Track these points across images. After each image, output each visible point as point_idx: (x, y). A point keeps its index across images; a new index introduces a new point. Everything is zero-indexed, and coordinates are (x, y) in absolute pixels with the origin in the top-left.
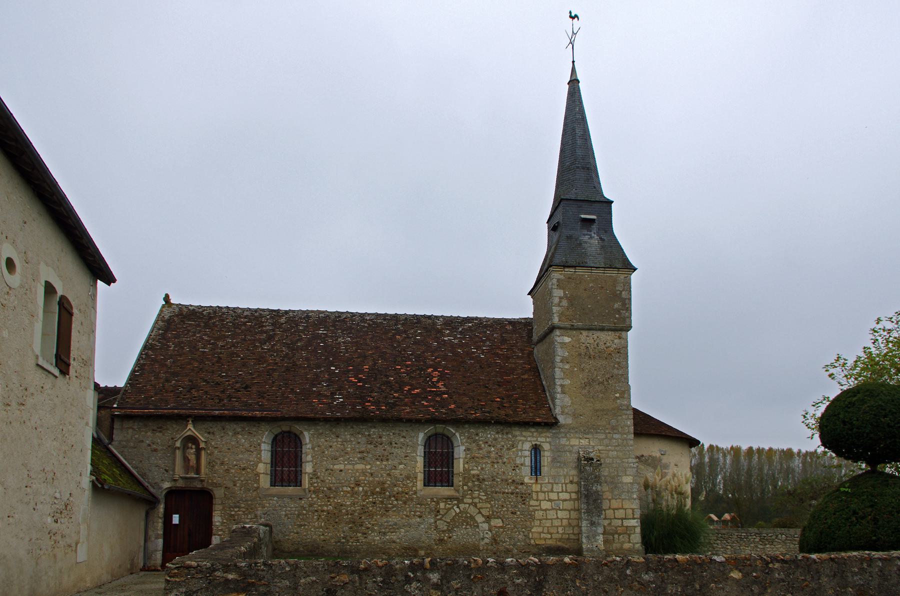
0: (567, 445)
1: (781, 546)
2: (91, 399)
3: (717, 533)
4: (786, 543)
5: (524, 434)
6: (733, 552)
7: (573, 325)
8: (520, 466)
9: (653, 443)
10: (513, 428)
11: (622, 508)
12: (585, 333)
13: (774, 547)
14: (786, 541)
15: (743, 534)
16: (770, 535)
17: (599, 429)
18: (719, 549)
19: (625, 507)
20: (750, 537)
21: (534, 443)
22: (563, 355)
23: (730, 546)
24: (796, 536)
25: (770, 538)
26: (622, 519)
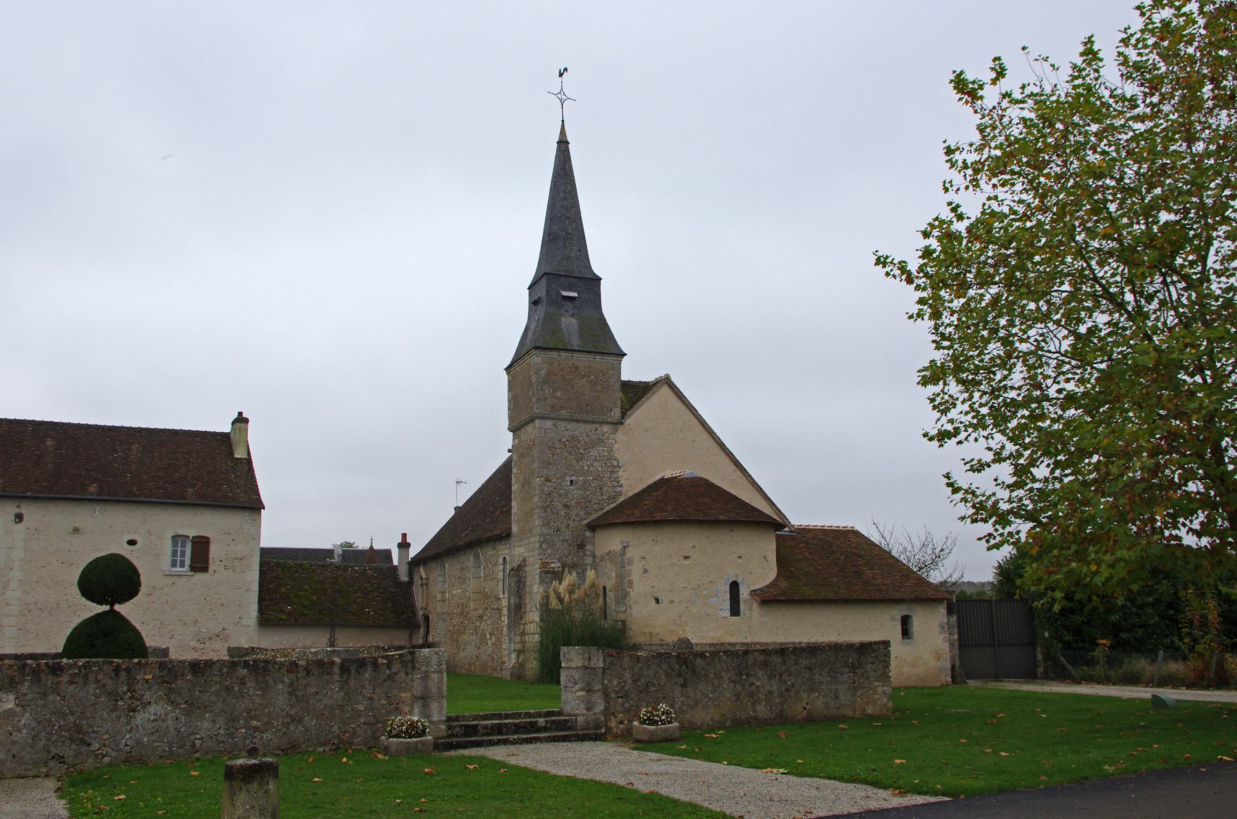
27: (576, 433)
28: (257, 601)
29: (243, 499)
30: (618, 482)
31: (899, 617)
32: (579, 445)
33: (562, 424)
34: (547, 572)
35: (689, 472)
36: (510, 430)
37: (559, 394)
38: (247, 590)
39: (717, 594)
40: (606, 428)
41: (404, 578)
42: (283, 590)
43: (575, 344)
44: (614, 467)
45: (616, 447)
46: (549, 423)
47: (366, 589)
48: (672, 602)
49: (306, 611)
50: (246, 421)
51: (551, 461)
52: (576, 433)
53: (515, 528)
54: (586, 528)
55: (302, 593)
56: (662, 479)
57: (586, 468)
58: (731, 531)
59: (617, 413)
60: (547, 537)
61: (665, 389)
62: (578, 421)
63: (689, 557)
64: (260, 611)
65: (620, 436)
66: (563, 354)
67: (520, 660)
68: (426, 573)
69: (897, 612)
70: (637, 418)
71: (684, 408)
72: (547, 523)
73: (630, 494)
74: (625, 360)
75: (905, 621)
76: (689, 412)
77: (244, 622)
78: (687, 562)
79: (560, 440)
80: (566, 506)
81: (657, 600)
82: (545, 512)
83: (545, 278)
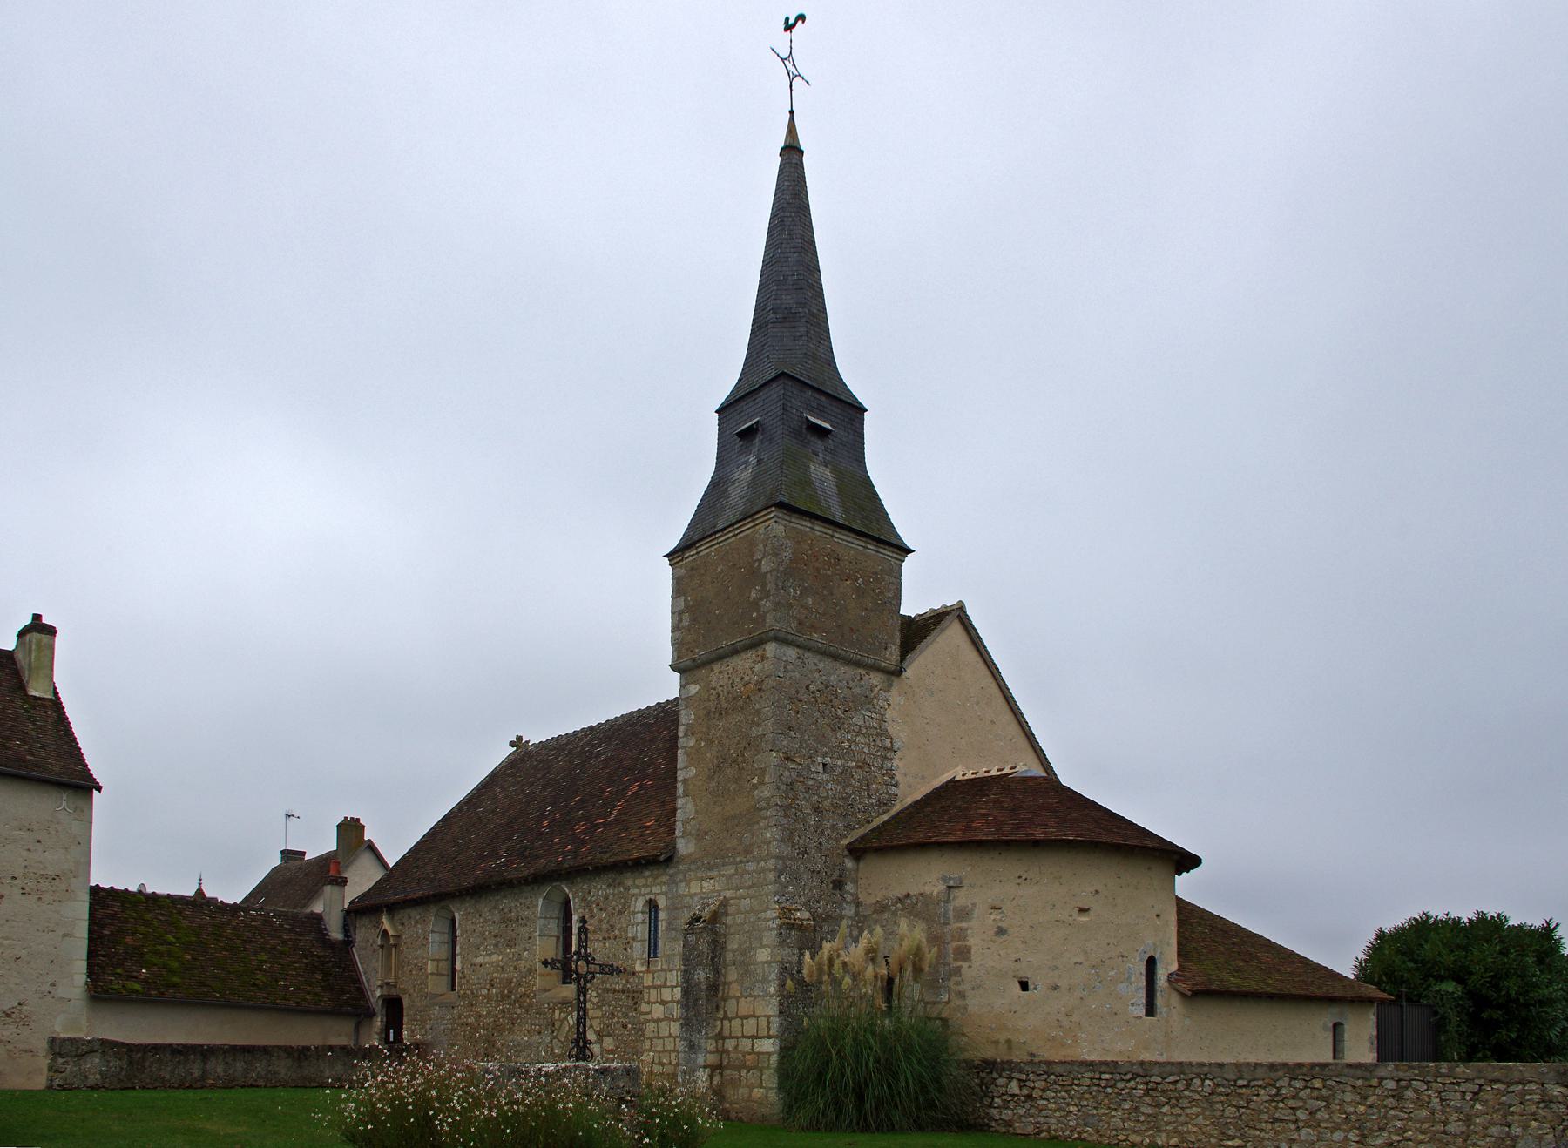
0: (686, 896)
1: (1199, 1110)
2: (80, 909)
3: (1045, 1073)
4: (1212, 1103)
5: (638, 882)
6: (1081, 1122)
7: (694, 660)
8: (631, 941)
9: (965, 860)
10: (625, 874)
11: (754, 1016)
12: (717, 667)
13: (1180, 1112)
14: (1215, 1098)
15: (1103, 1076)
16: (1171, 1079)
17: (728, 857)
18: (1050, 1112)
19: (757, 1013)
20: (1120, 1085)
21: (648, 897)
22: (687, 722)
23: (1075, 1105)
24: (1240, 1082)
25: (1171, 1087)
26: (753, 1038)
27: (832, 678)
28: (85, 957)
29: (57, 769)
30: (892, 778)
31: (1331, 1025)
32: (836, 702)
33: (811, 659)
34: (791, 927)
35: (1025, 768)
36: (674, 667)
37: (810, 601)
38: (65, 935)
39: (1129, 977)
40: (876, 679)
41: (336, 934)
42: (128, 939)
43: (837, 514)
44: (886, 748)
45: (889, 714)
46: (791, 653)
47: (274, 948)
48: (1055, 988)
49: (176, 979)
50: (51, 631)
51: (793, 724)
52: (832, 678)
53: (684, 847)
54: (846, 853)
55: (163, 948)
56: (951, 781)
57: (846, 745)
58: (1149, 869)
59: (894, 653)
60: (789, 863)
61: (954, 630)
62: (835, 657)
63: (1088, 910)
64: (91, 973)
65: (894, 696)
66: (820, 528)
67: (715, 1082)
68: (394, 927)
69: (1328, 1017)
70: (918, 666)
71: (981, 665)
72: (788, 839)
73: (909, 801)
74: (909, 564)
75: (1337, 1027)
76: (988, 673)
77: (61, 992)
78: (1084, 919)
79: (807, 688)
80: (817, 810)
81: (1024, 986)
82: (786, 816)
83: (776, 390)
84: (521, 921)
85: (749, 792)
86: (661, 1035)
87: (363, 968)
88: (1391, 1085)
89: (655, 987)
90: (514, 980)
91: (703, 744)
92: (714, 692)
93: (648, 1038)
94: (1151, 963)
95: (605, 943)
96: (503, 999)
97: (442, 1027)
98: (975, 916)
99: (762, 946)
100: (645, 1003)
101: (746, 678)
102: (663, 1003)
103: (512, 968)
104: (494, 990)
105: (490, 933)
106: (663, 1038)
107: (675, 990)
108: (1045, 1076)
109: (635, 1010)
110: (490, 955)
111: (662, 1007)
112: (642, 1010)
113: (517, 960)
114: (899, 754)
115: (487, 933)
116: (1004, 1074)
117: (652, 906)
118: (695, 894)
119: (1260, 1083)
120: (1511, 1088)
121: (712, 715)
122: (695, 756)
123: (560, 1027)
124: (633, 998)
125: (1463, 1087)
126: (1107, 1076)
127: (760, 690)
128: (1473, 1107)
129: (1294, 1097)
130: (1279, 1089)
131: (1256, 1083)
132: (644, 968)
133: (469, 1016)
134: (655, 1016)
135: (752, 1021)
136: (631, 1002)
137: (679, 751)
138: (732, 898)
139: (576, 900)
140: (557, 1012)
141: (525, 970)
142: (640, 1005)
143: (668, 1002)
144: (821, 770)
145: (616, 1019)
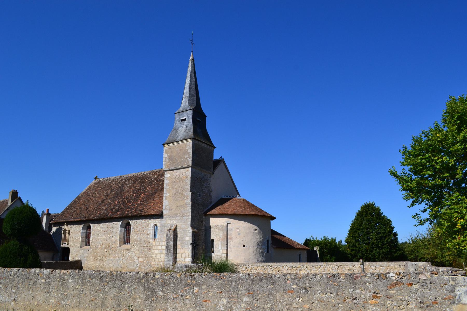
0: (166, 224)
7: (170, 169)
15: (264, 266)
16: (279, 266)
19: (186, 252)
21: (154, 224)
24: (294, 267)
25: (279, 268)
26: (184, 258)
31: (299, 255)
79: (197, 178)
84: (113, 228)
85: (184, 201)
86: (157, 258)
87: (54, 239)
88: (323, 267)
89: (156, 246)
90: (111, 243)
91: (171, 188)
92: (174, 177)
93: (154, 258)
94: (268, 241)
95: (141, 234)
96: (106, 248)
97: (84, 256)
98: (233, 230)
99: (187, 236)
100: (153, 250)
101: (183, 175)
102: (158, 250)
103: (110, 240)
104: (103, 246)
105: (102, 230)
106: (158, 258)
107: (162, 246)
108: (251, 266)
109: (150, 251)
110: (102, 237)
111: (158, 251)
112: (152, 251)
113: (112, 238)
114: (213, 192)
115: (101, 231)
116: (242, 266)
117: (155, 226)
118: (168, 223)
119: (297, 267)
120: (344, 267)
121: (174, 182)
122: (168, 191)
123: (126, 256)
124: (149, 248)
125: (336, 267)
126: (265, 266)
127: (187, 178)
128: (337, 271)
129: (304, 270)
130: (301, 268)
131: (297, 267)
132: (153, 241)
133: (94, 253)
134: (156, 253)
135: (184, 254)
136: (149, 249)
137: (164, 189)
138: (179, 225)
139: (132, 223)
140: (125, 252)
141: (115, 241)
142: (151, 250)
143: (160, 249)
144: (199, 196)
145: (144, 254)
